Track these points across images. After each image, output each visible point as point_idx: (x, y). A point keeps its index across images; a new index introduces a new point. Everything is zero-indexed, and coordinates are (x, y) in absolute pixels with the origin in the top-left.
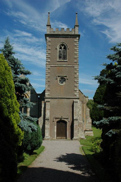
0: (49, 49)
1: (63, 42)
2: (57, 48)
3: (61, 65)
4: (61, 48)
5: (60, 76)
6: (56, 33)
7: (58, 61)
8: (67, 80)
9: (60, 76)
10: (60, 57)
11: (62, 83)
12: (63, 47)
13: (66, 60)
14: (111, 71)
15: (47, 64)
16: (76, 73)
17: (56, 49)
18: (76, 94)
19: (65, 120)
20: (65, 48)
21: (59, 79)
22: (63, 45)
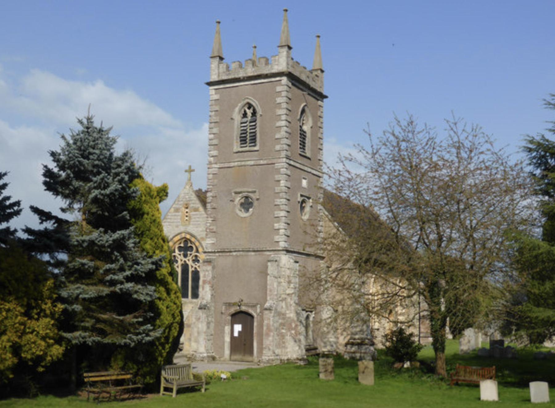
0: (215, 123)
1: (247, 98)
2: (233, 117)
3: (243, 163)
4: (245, 115)
5: (240, 193)
6: (303, 77)
7: (237, 153)
8: (256, 203)
9: (240, 193)
10: (243, 140)
11: (247, 210)
12: (251, 111)
13: (255, 148)
14: (444, 241)
15: (210, 163)
16: (278, 242)
17: (232, 119)
18: (277, 238)
19: (251, 311)
20: (254, 113)
21: (238, 199)
22: (250, 106)
